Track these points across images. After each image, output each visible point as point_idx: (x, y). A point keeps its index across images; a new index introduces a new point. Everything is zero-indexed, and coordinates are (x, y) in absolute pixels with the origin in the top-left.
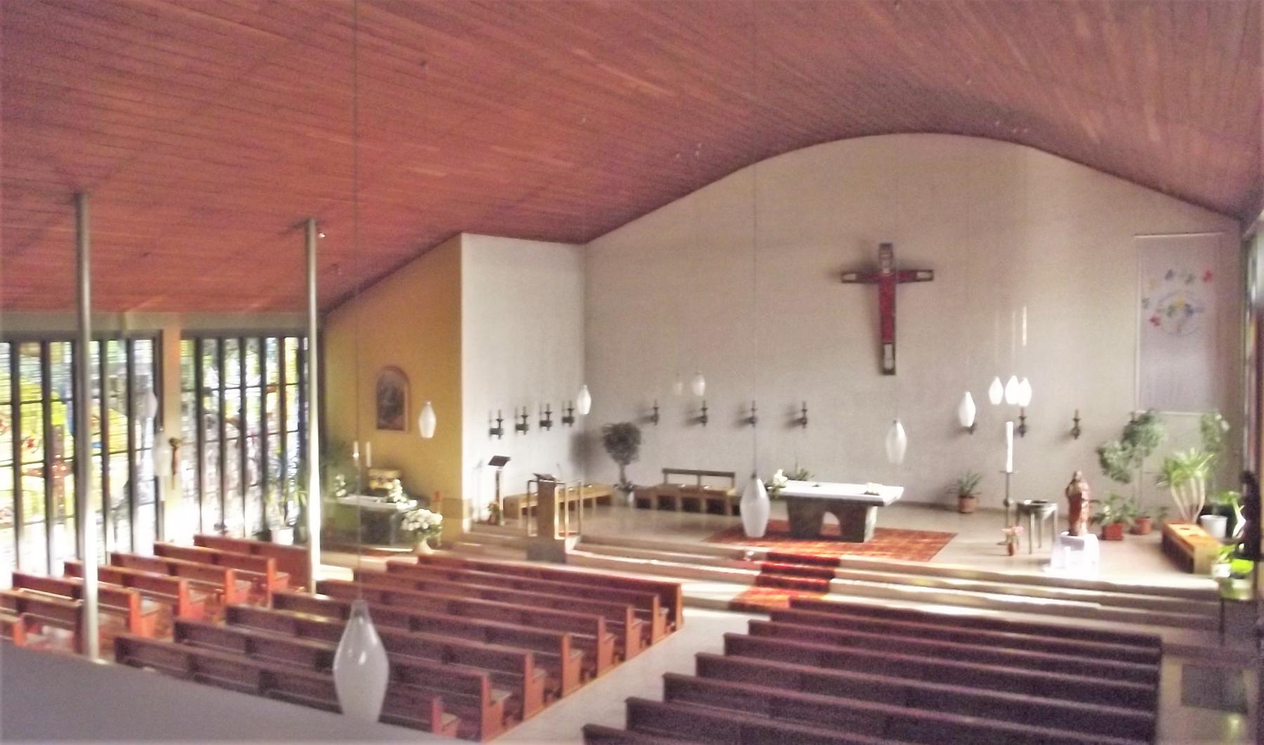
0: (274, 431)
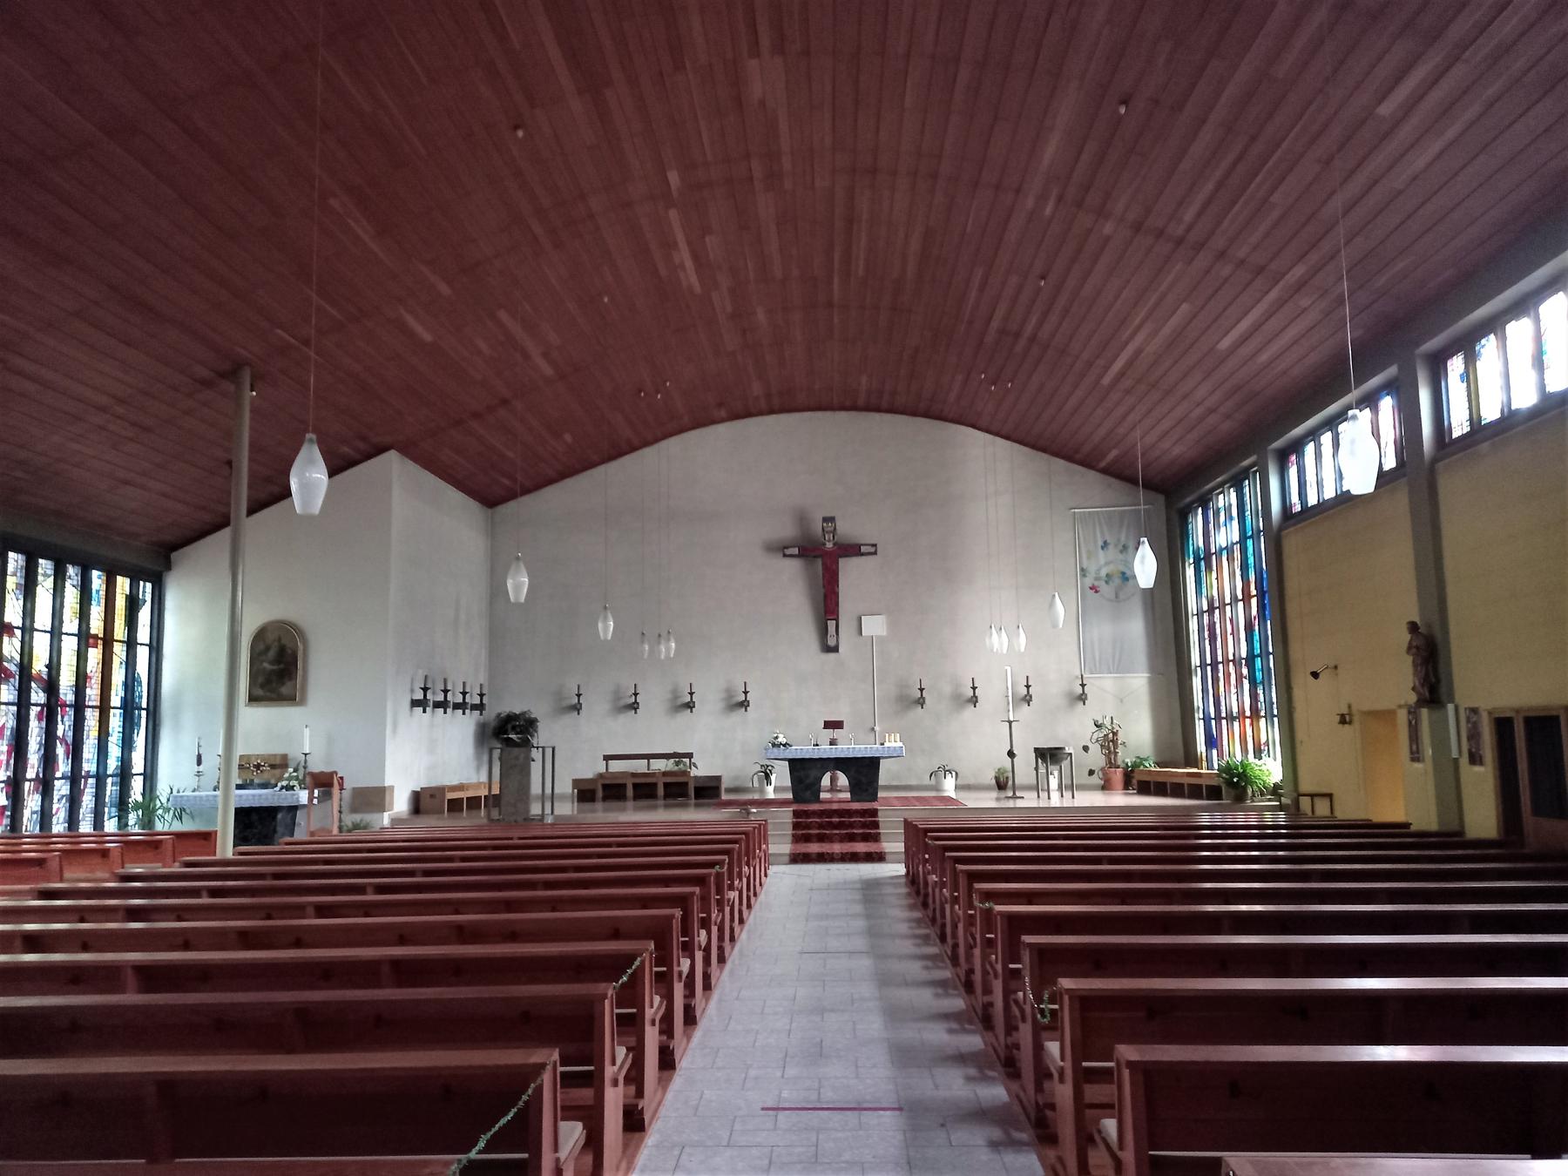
0: (94, 704)
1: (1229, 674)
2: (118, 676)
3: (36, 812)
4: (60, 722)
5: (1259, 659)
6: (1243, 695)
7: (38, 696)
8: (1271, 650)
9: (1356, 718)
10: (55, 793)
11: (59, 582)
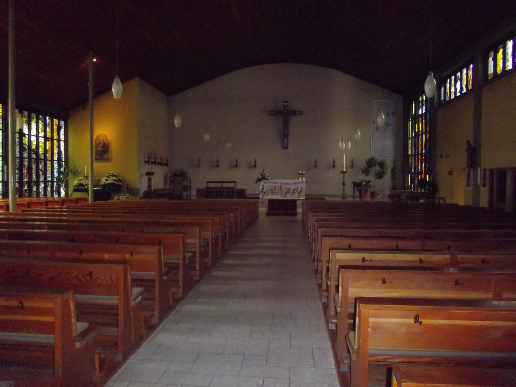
2: (56, 151)
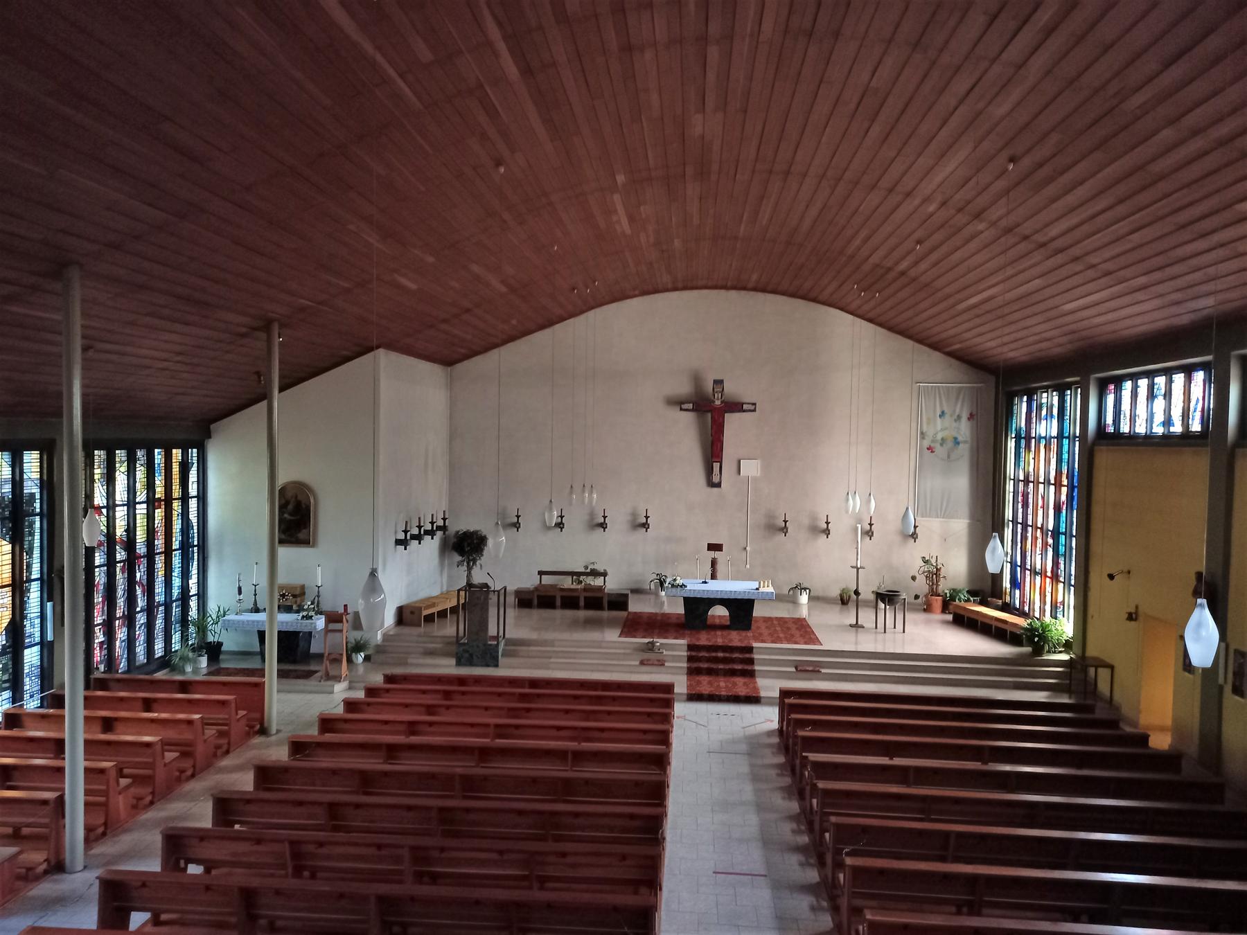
1: (1036, 538)
2: (177, 525)
3: (124, 641)
4: (137, 571)
5: (1064, 536)
6: (1046, 559)
7: (121, 555)
8: (1074, 534)
9: (1141, 618)
10: (137, 623)
11: (132, 465)
